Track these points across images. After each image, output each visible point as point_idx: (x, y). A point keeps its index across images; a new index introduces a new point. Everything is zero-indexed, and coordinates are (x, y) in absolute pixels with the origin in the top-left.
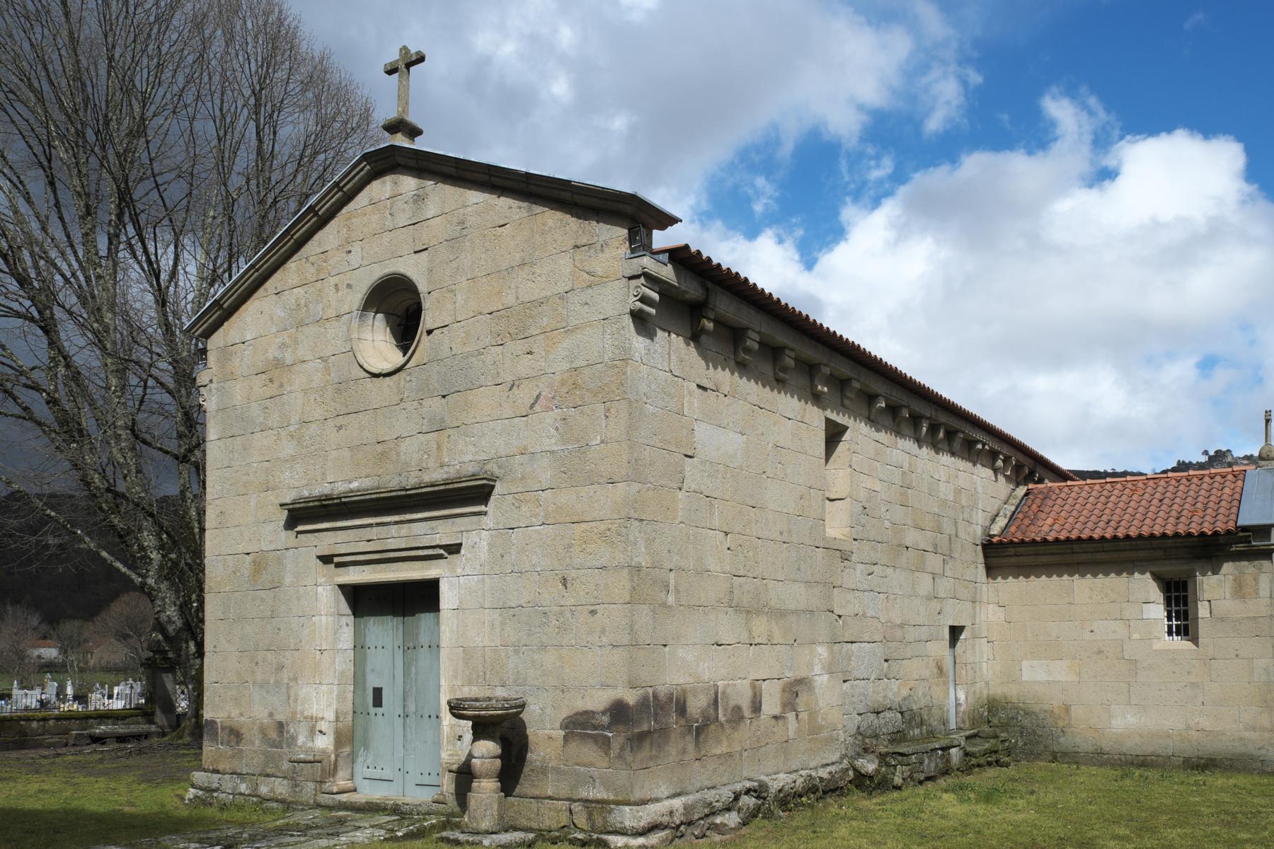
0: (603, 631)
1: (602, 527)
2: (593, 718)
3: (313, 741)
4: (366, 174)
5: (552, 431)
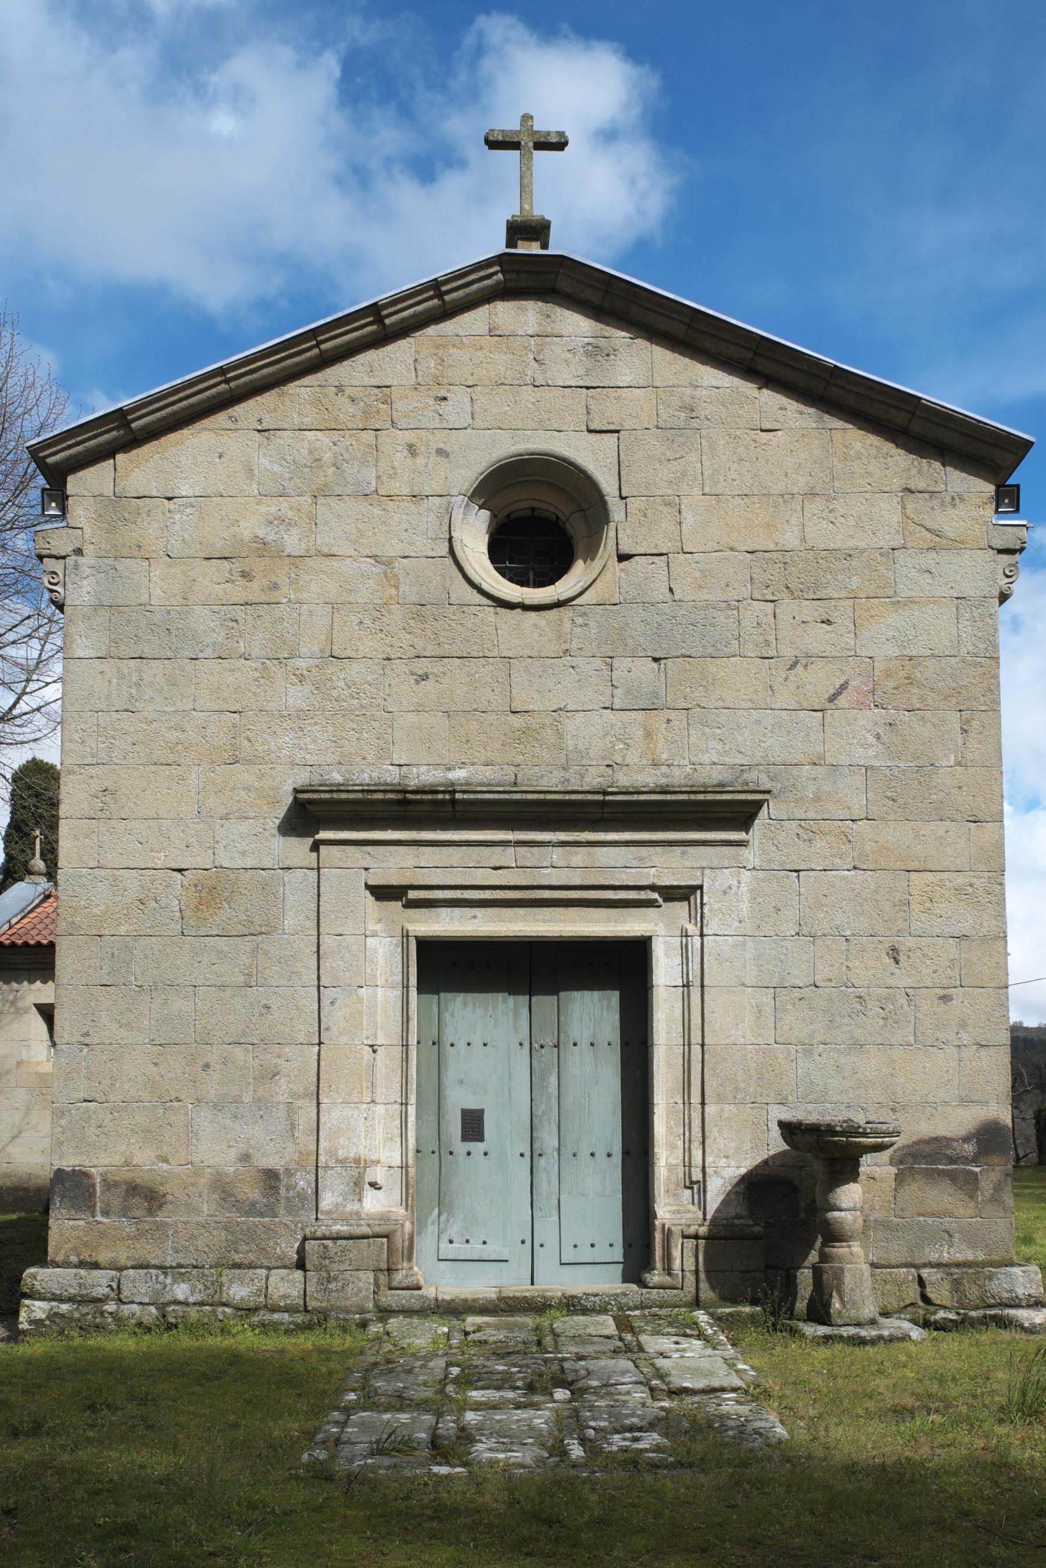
0: (963, 1025)
1: (960, 880)
2: (948, 1146)
3: (360, 1200)
4: (492, 286)
5: (871, 739)
